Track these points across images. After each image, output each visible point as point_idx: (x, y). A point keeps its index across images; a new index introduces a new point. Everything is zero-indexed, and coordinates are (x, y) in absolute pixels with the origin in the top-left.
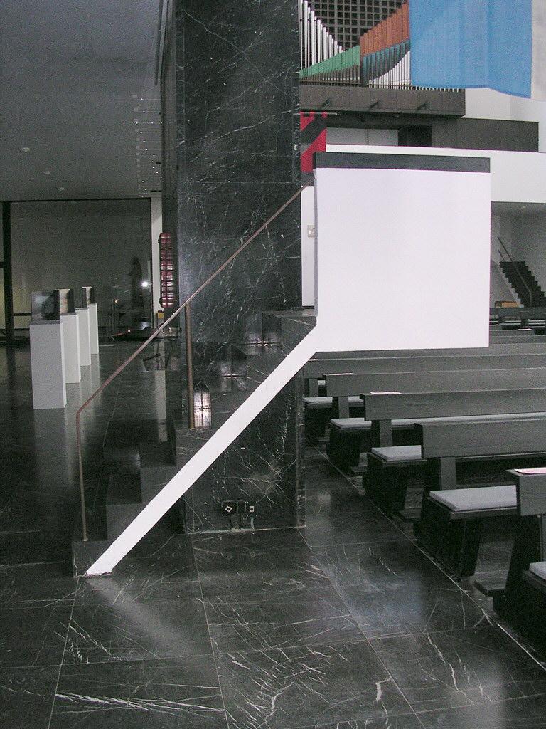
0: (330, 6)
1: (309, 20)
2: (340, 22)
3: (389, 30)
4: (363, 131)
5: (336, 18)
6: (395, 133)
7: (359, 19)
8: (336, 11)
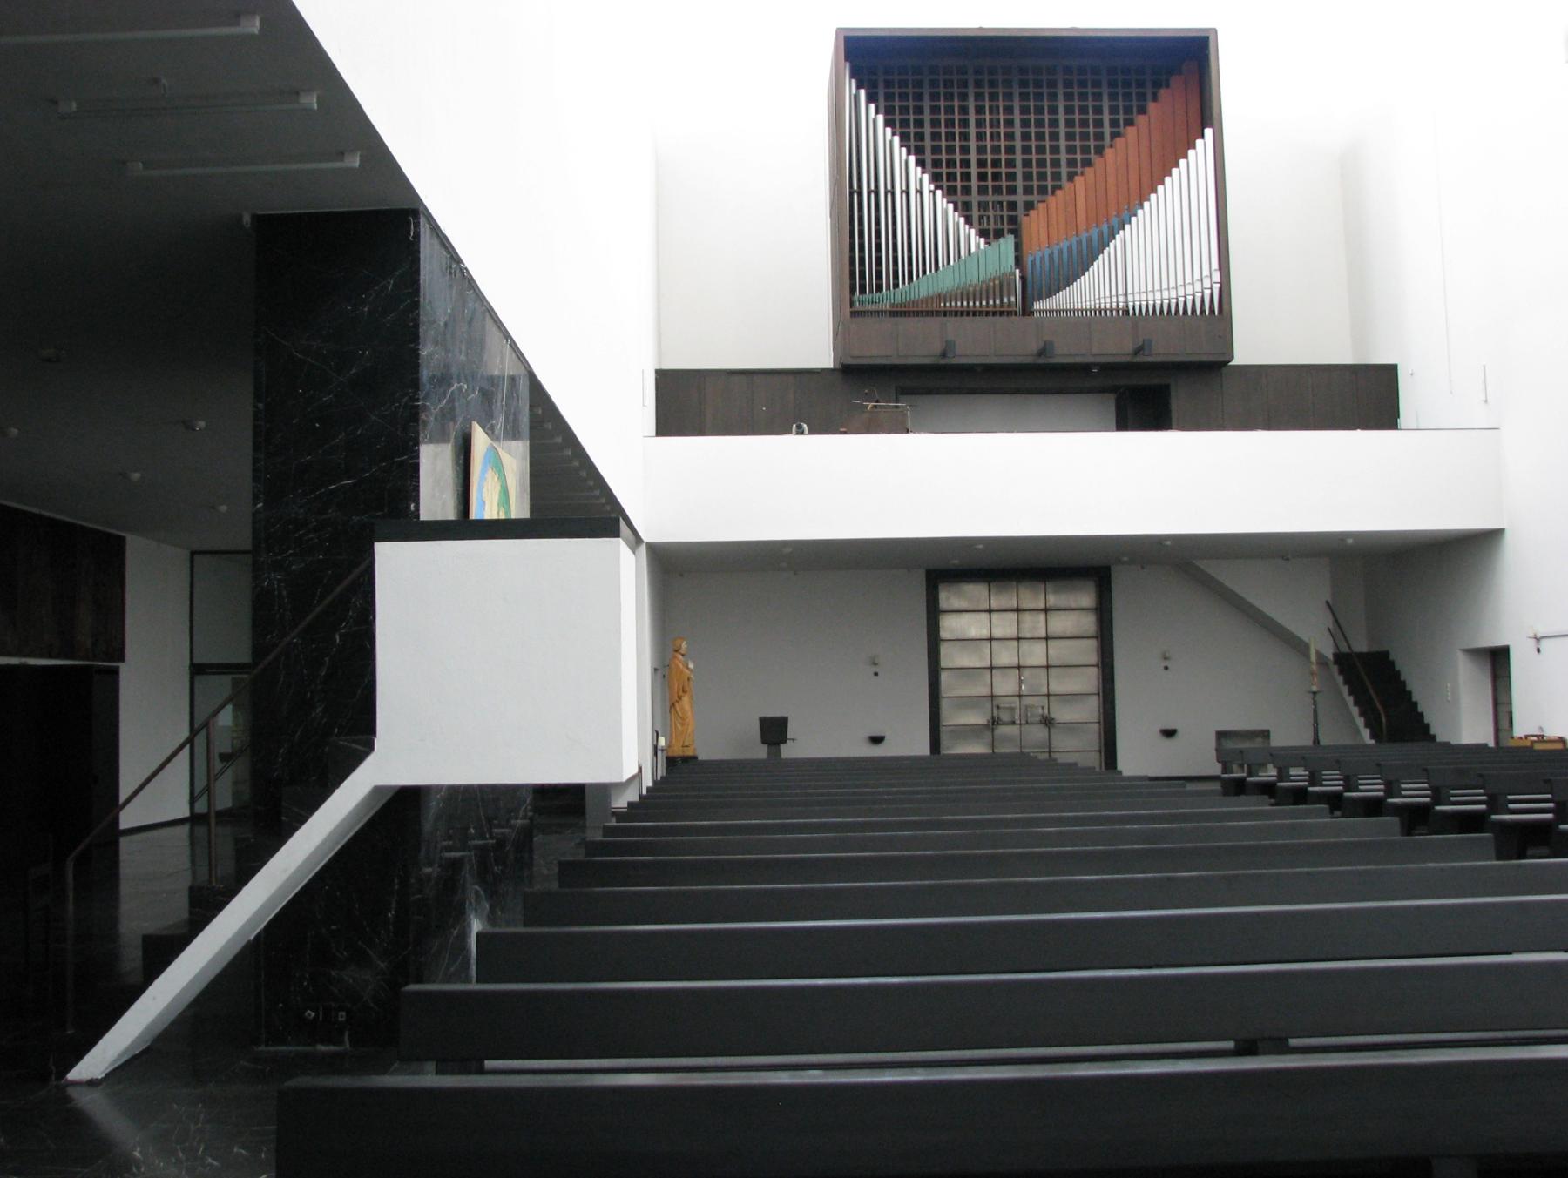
1: (920, 192)
6: (1108, 405)
7: (1020, 183)
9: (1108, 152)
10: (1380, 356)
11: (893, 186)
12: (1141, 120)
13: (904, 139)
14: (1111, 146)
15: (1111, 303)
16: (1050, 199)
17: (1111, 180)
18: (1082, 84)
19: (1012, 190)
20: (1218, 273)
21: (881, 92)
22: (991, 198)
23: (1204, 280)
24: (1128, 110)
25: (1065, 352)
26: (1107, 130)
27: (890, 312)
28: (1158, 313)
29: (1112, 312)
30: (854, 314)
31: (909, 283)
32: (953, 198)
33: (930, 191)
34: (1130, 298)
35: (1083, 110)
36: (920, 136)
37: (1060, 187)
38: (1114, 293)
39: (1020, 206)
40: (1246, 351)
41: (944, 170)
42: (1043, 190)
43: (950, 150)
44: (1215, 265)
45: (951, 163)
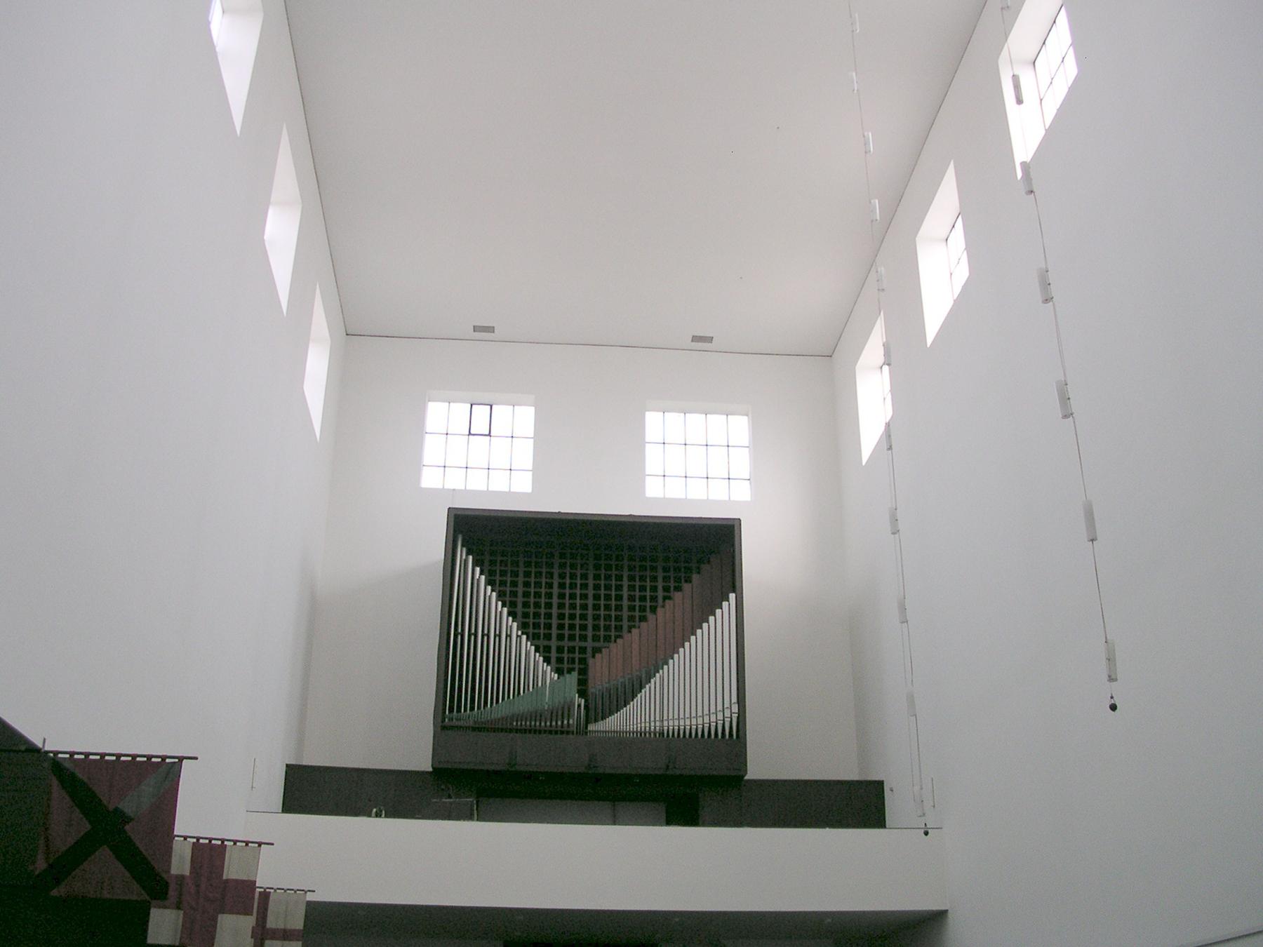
0: (575, 608)
1: (509, 636)
2: (560, 637)
3: (635, 646)
4: (607, 805)
5: (554, 632)
6: (662, 808)
7: (590, 633)
8: (555, 622)
9: (659, 610)
10: (874, 776)
11: (500, 632)
12: (686, 587)
13: (500, 596)
14: (663, 606)
15: (637, 728)
16: (612, 645)
17: (661, 632)
18: (608, 557)
19: (583, 638)
20: (737, 705)
21: (487, 558)
22: (566, 643)
23: (726, 710)
24: (678, 580)
25: (610, 764)
26: (660, 594)
27: (472, 727)
28: (682, 736)
29: (650, 734)
30: (444, 728)
31: (484, 708)
32: (537, 642)
33: (517, 636)
34: (665, 723)
35: (608, 577)
36: (514, 594)
37: (620, 637)
38: (652, 719)
39: (589, 650)
40: (757, 769)
41: (531, 620)
42: (607, 639)
43: (537, 605)
44: (734, 699)
45: (537, 615)
